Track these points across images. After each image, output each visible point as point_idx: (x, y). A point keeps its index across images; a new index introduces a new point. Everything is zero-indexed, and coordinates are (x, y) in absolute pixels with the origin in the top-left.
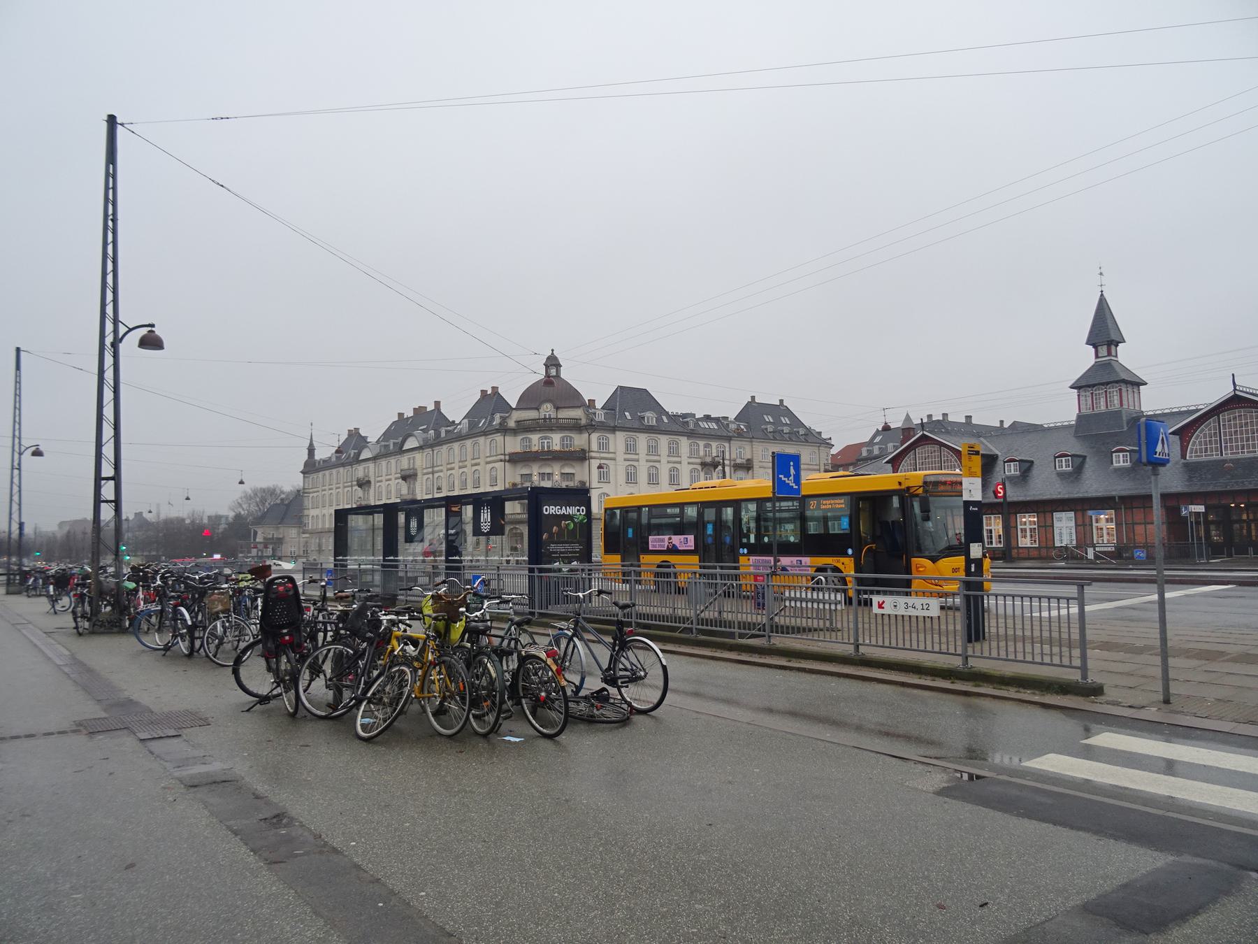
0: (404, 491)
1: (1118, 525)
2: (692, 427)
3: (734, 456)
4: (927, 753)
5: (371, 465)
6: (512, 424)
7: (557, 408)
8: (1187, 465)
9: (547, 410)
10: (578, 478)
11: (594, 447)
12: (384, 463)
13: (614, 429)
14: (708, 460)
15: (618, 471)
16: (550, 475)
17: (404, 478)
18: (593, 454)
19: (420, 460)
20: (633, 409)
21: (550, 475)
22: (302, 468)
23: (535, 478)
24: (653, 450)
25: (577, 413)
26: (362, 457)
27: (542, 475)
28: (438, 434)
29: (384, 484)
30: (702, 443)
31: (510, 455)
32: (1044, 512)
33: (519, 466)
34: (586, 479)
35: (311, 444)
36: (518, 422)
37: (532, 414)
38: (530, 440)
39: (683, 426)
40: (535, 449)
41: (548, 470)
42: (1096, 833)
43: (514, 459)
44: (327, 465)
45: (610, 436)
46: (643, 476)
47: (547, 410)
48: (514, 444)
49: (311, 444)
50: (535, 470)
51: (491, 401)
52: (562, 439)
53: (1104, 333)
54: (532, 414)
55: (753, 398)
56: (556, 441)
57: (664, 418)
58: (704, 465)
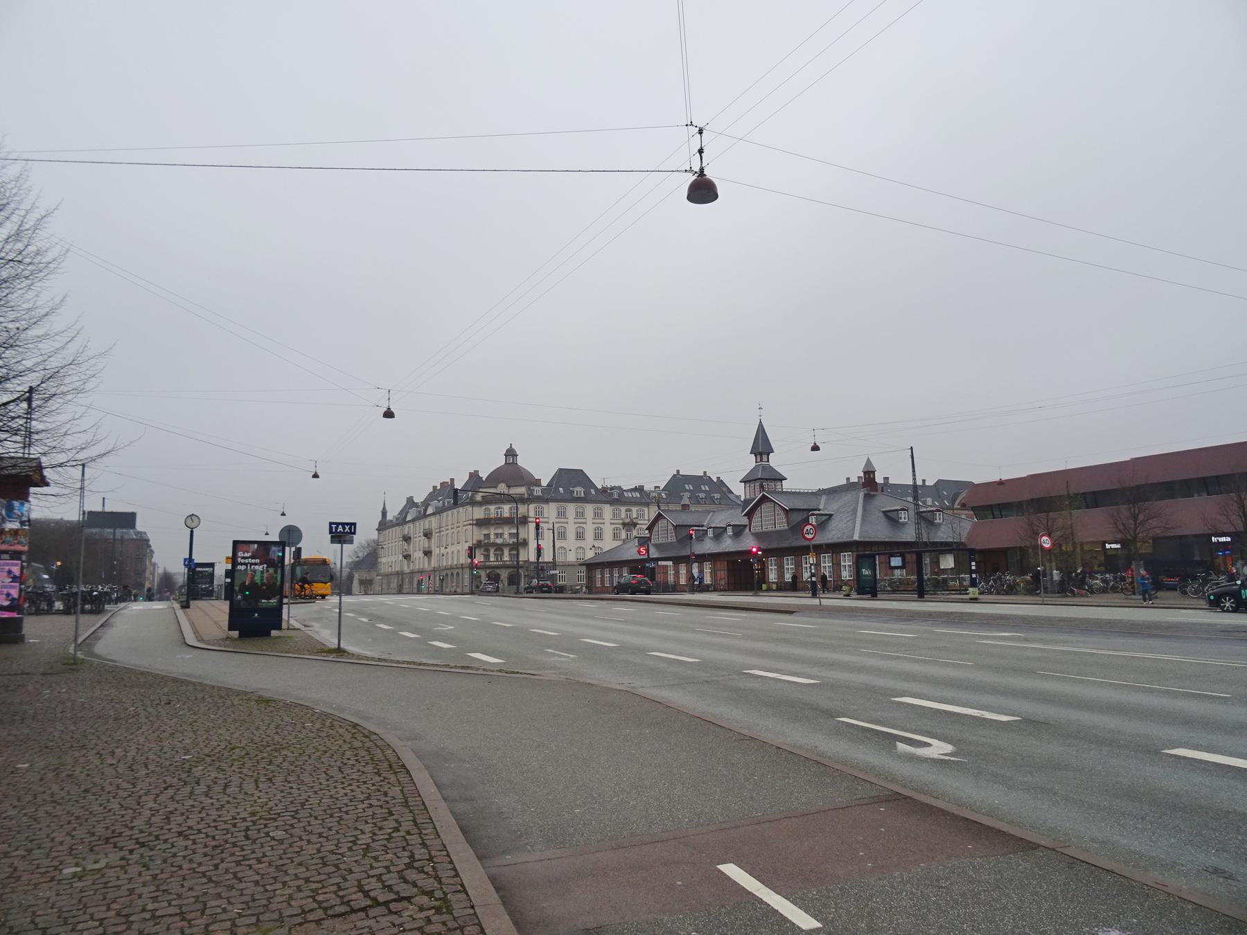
2: (616, 496)
4: (556, 658)
5: (411, 525)
6: (479, 497)
7: (509, 487)
11: (532, 514)
13: (547, 501)
14: (627, 521)
16: (501, 535)
20: (571, 486)
21: (501, 535)
24: (580, 514)
25: (522, 490)
27: (497, 535)
30: (623, 509)
40: (492, 516)
41: (500, 531)
43: (480, 523)
45: (544, 506)
46: (589, 534)
47: (502, 488)
48: (479, 513)
50: (492, 531)
51: (474, 476)
53: (762, 447)
56: (506, 510)
57: (593, 492)
58: (624, 524)
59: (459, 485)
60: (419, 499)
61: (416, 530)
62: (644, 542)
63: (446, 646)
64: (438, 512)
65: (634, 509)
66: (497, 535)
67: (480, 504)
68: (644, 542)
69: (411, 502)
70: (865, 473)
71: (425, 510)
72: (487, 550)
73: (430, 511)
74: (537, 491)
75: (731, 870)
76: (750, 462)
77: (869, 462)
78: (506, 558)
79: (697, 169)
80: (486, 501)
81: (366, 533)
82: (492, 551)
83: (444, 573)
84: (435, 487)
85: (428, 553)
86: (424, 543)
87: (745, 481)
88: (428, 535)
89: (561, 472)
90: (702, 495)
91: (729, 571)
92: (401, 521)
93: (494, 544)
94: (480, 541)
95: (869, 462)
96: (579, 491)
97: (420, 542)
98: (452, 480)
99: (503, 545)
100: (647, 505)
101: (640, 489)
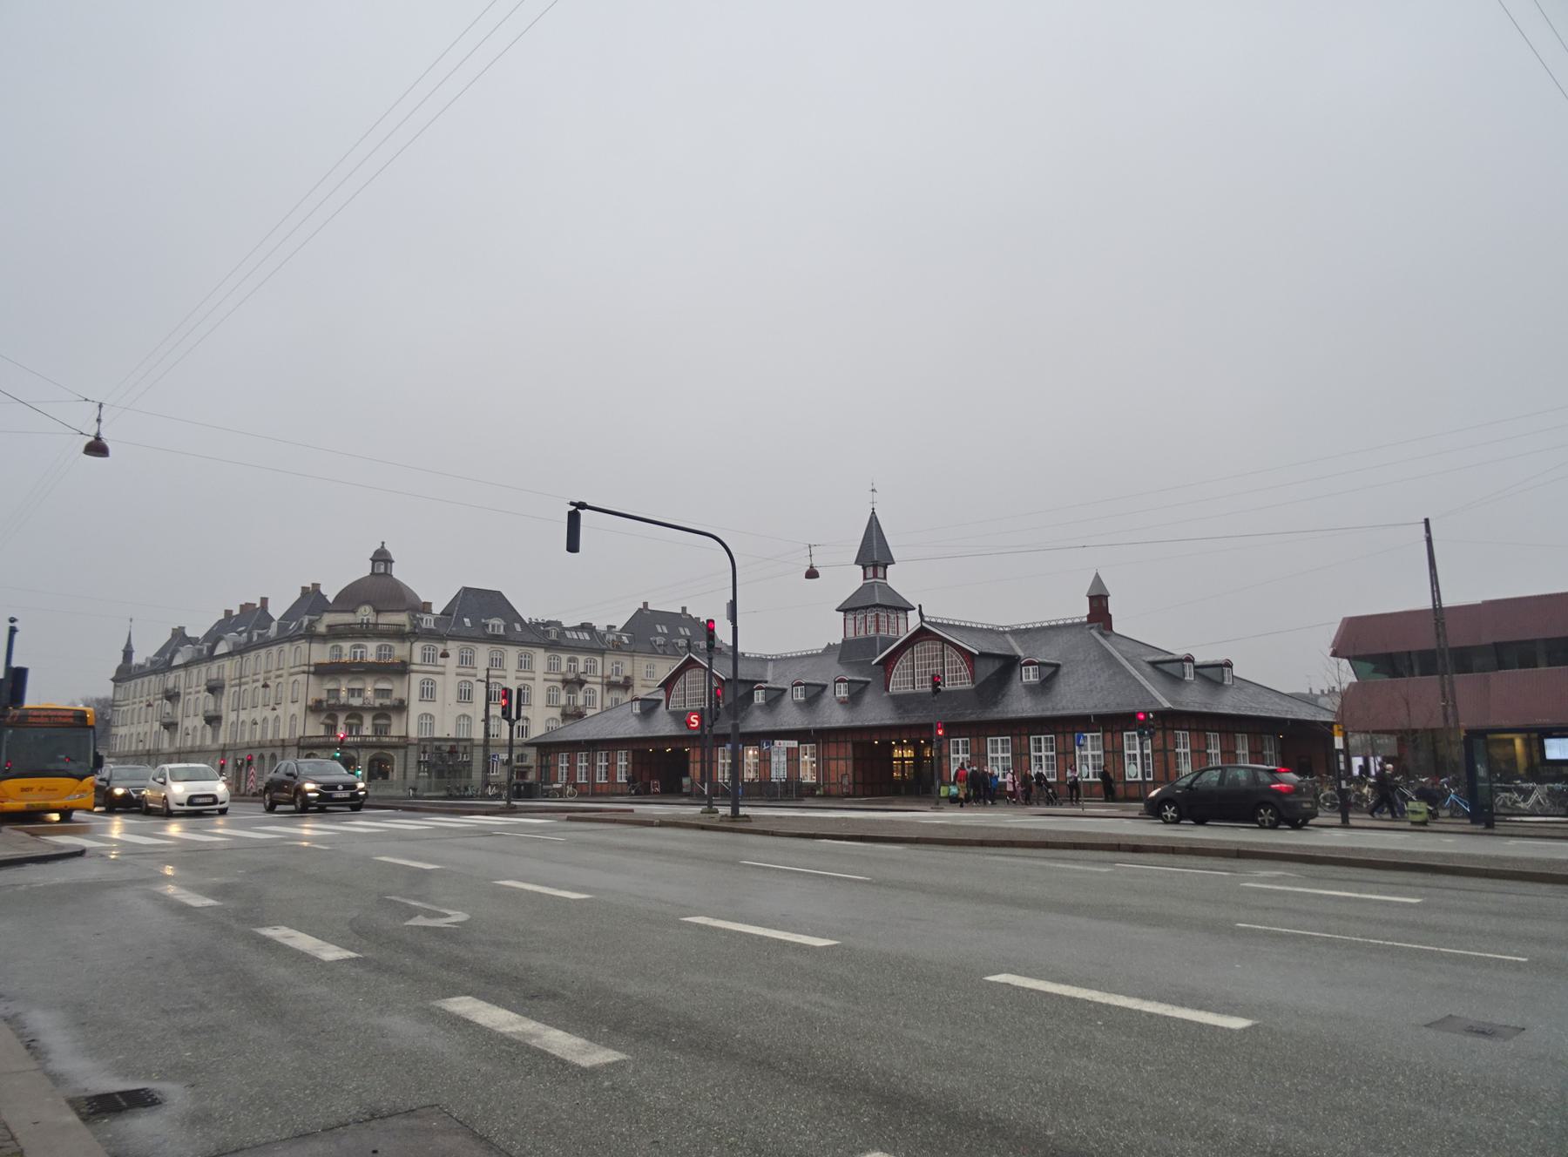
0: (211, 707)
1: (818, 762)
2: (553, 637)
3: (607, 672)
5: (182, 673)
6: (321, 628)
7: (378, 612)
8: (672, 713)
9: (365, 614)
10: (396, 695)
11: (417, 658)
12: (195, 671)
13: (442, 638)
14: (571, 676)
15: (448, 686)
16: (361, 691)
17: (169, 698)
18: (414, 667)
19: (229, 669)
20: (481, 615)
21: (361, 691)
22: (113, 675)
23: (343, 694)
25: (402, 618)
26: (217, 653)
27: (352, 692)
28: (250, 638)
29: (192, 697)
30: (564, 657)
31: (317, 665)
32: (1064, 733)
33: (326, 679)
34: (405, 696)
35: (129, 645)
36: (329, 627)
37: (347, 618)
38: (341, 649)
39: (547, 637)
40: (345, 659)
41: (357, 685)
42: (546, 1053)
43: (322, 671)
44: (142, 672)
47: (365, 614)
48: (321, 653)
49: (129, 645)
50: (344, 685)
51: (312, 599)
52: (380, 648)
53: (874, 553)
54: (347, 618)
55: (645, 604)
56: (371, 651)
57: (518, 627)
58: (566, 682)
59: (277, 611)
60: (197, 630)
61: (192, 683)
62: (649, 708)
63: (1238, 1023)
64: (238, 651)
65: (582, 659)
66: (352, 692)
67: (323, 638)
68: (649, 708)
69: (179, 636)
70: (1091, 598)
71: (212, 649)
72: (333, 717)
73: (178, 660)
74: (428, 622)
75: (331, 953)
76: (854, 579)
77: (1098, 580)
78: (367, 730)
79: (93, 433)
80: (335, 634)
81: (441, 661)
82: (341, 719)
83: (245, 755)
84: (228, 613)
85: (213, 720)
86: (209, 703)
87: (845, 609)
88: (215, 689)
89: (466, 591)
90: (660, 640)
91: (855, 760)
92: (162, 664)
93: (346, 708)
94: (319, 702)
95: (1098, 580)
96: (497, 624)
97: (197, 701)
98: (264, 601)
99: (363, 709)
100: (602, 652)
101: (586, 627)
